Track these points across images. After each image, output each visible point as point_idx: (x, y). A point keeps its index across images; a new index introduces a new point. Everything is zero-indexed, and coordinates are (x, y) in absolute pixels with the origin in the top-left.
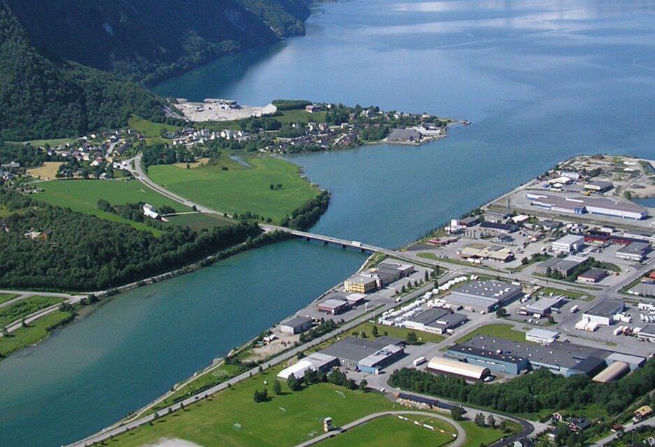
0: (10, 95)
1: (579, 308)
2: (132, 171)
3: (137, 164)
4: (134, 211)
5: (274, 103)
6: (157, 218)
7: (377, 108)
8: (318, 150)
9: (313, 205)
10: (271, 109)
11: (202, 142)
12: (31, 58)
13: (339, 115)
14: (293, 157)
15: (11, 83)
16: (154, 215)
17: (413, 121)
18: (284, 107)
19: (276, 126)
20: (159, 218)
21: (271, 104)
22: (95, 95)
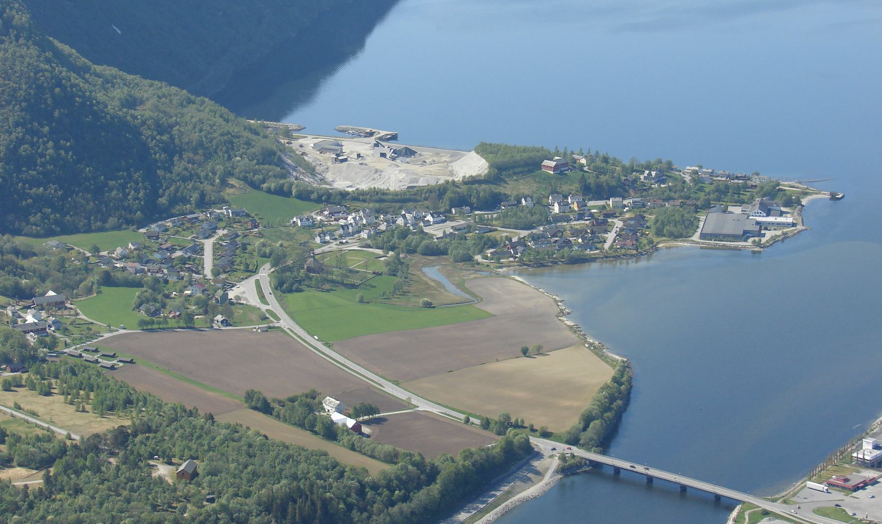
0: (16, 148)
1: (136, 312)
2: (264, 308)
3: (267, 290)
4: (306, 413)
5: (483, 150)
6: (354, 428)
7: (669, 164)
8: (579, 261)
9: (612, 399)
10: (473, 165)
11: (366, 236)
12: (47, 74)
13: (604, 182)
14: (534, 275)
15: (17, 124)
16: (351, 423)
17: (731, 192)
18: (512, 165)
19: (493, 202)
20: (357, 428)
21: (473, 152)
22: (163, 142)
